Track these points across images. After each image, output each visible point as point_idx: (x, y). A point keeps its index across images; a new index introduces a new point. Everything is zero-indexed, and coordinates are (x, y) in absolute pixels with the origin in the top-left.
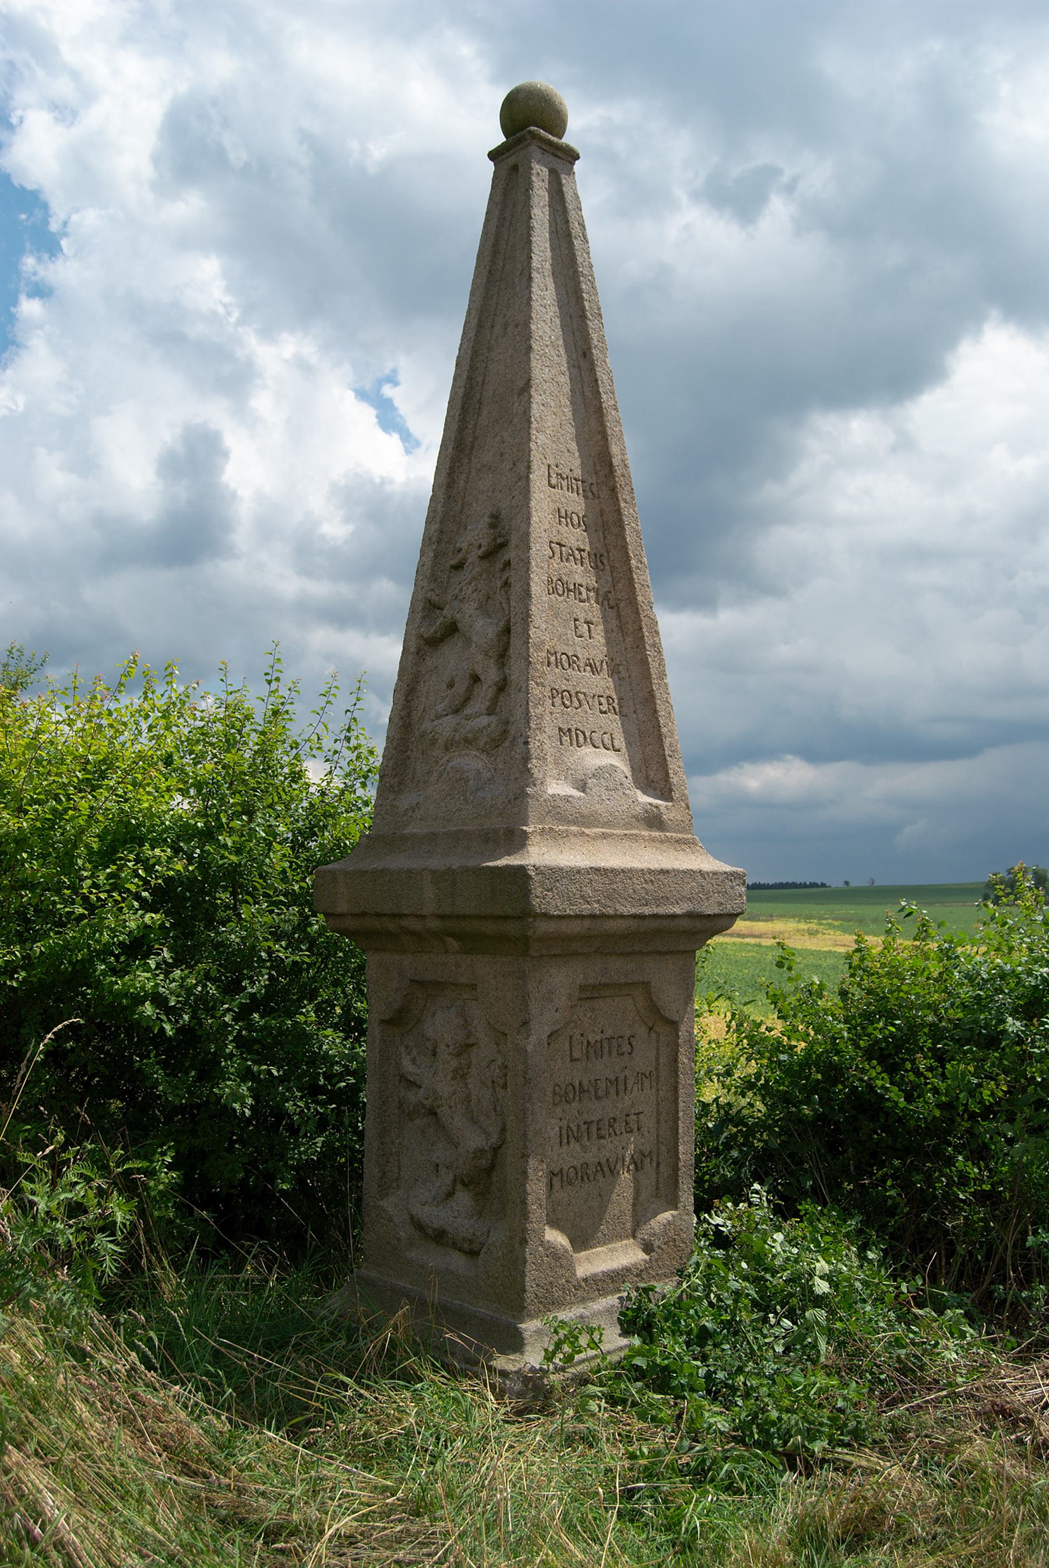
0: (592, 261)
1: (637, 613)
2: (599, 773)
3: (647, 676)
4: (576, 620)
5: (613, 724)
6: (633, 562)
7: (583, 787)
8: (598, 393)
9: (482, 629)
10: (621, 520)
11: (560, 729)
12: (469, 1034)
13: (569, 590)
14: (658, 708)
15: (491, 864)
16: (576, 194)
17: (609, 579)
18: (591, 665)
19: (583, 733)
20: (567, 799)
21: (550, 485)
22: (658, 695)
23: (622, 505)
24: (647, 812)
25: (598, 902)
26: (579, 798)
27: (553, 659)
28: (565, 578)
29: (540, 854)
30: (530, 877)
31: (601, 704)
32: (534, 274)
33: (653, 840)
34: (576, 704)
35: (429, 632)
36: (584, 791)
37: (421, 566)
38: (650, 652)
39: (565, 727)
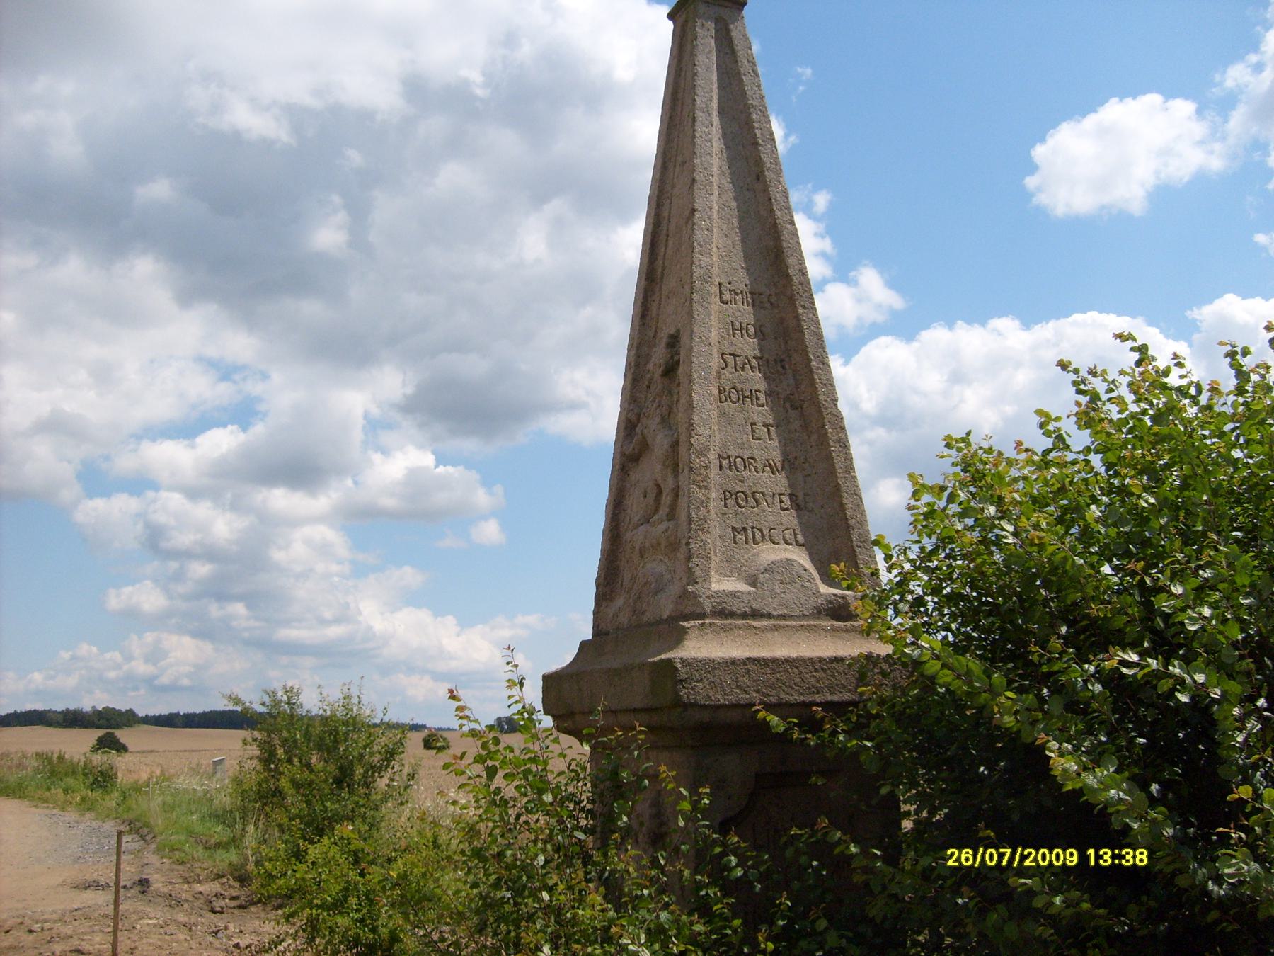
0: (764, 93)
1: (820, 412)
2: (770, 569)
3: (832, 471)
4: (752, 424)
5: (790, 519)
6: (814, 363)
7: (753, 581)
8: (772, 211)
9: (660, 442)
10: (799, 325)
11: (734, 529)
12: (662, 824)
13: (744, 397)
14: (845, 501)
15: (656, 659)
16: (745, 35)
17: (792, 381)
18: (770, 466)
19: (760, 530)
20: (734, 595)
21: (722, 301)
22: (844, 489)
23: (801, 311)
24: (830, 602)
25: (758, 691)
26: (749, 593)
27: (725, 462)
28: (739, 386)
29: (700, 647)
30: (677, 669)
31: (781, 502)
32: (699, 114)
33: (834, 629)
34: (752, 502)
35: (629, 449)
36: (755, 586)
37: (624, 389)
38: (834, 448)
39: (739, 526)
